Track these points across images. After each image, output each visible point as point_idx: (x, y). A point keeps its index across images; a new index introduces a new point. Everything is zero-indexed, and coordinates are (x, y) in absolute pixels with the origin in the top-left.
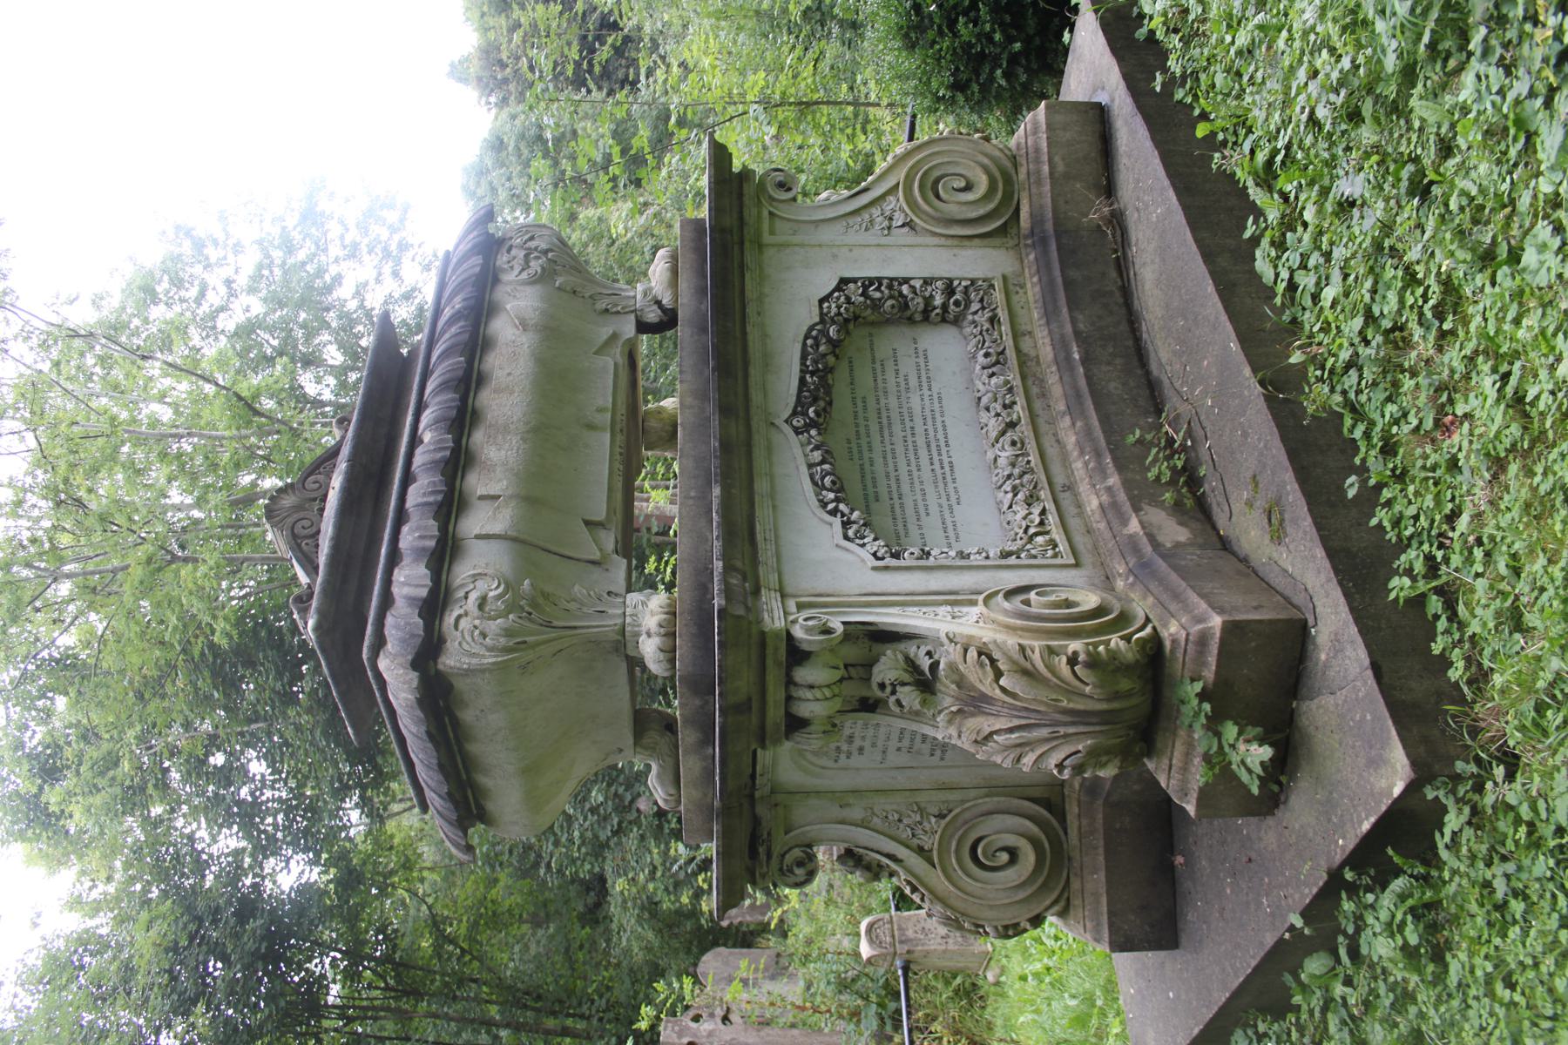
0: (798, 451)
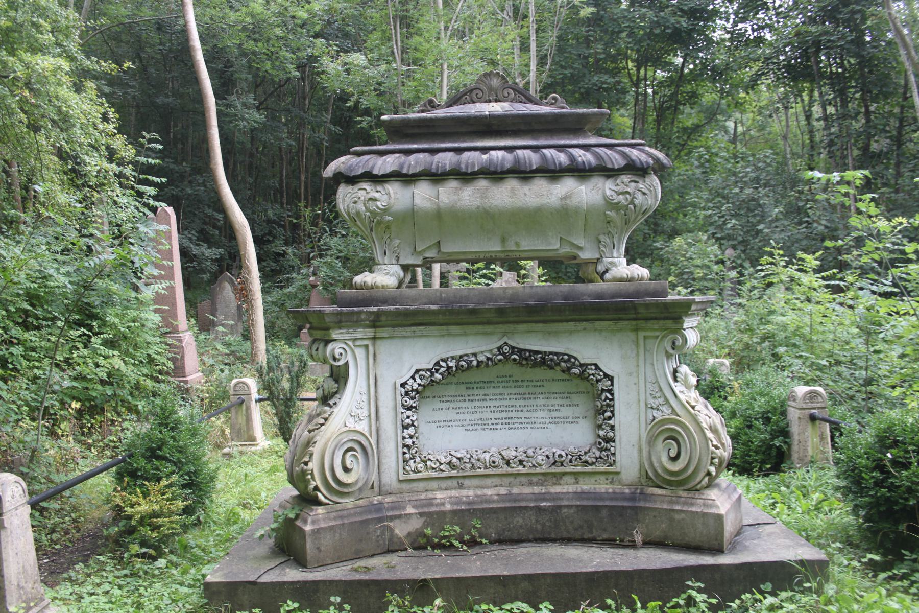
0: (483, 349)
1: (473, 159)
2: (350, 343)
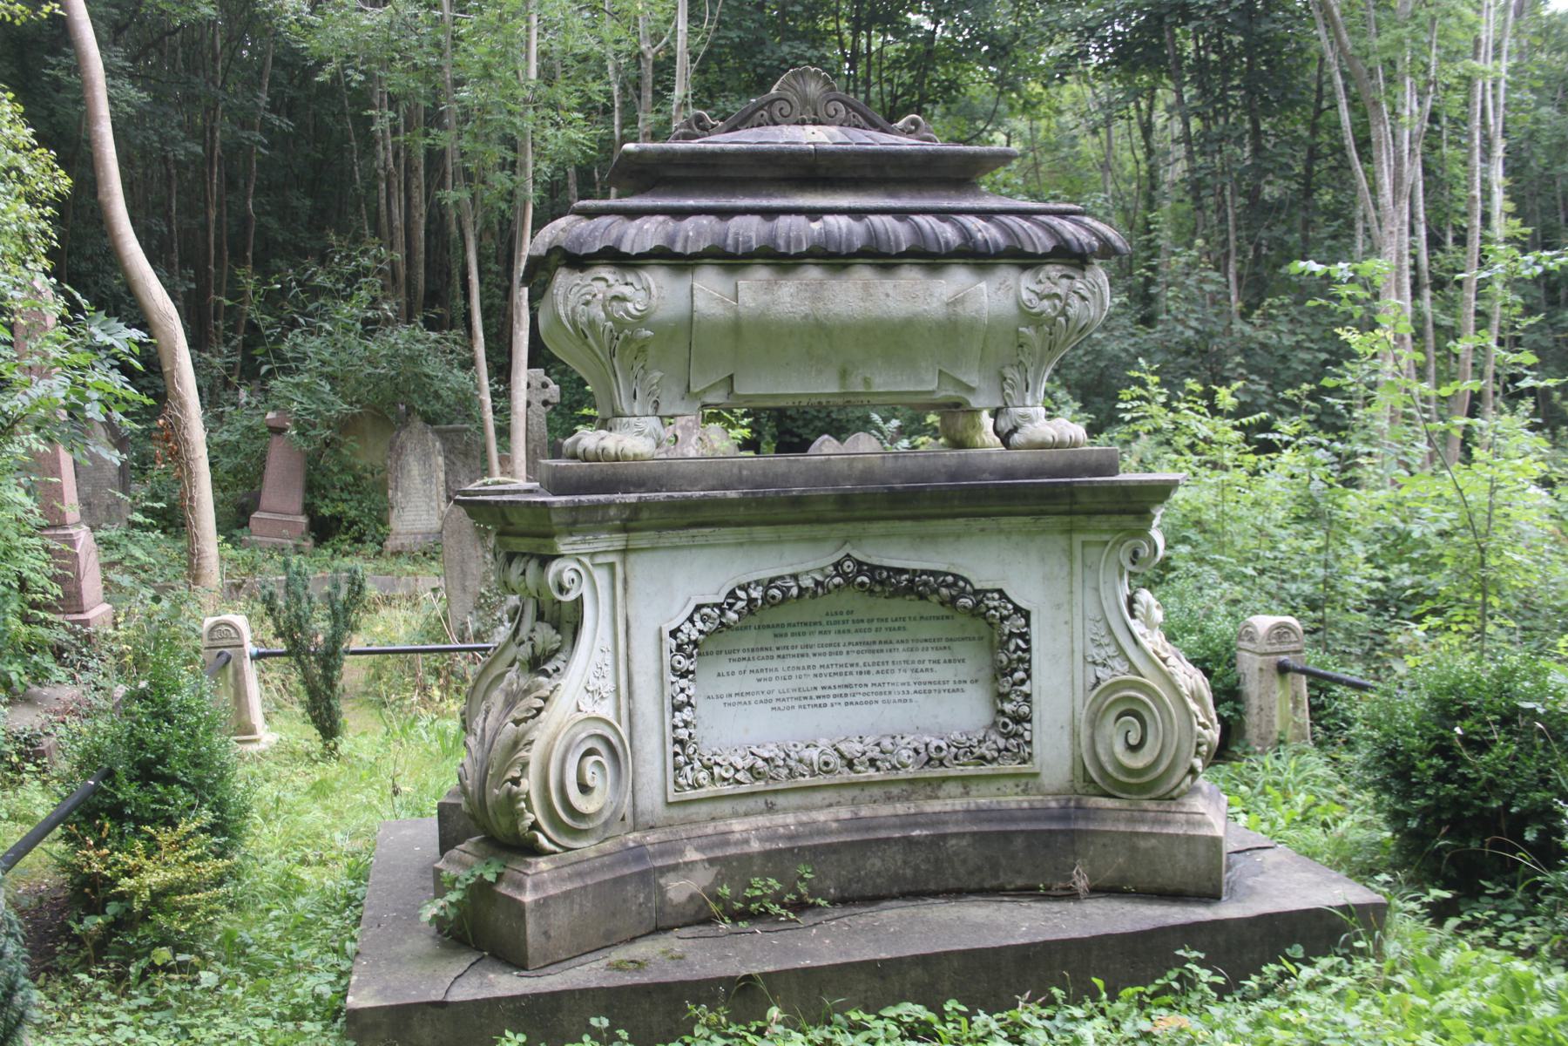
0: (810, 566)
1: (795, 230)
2: (586, 560)
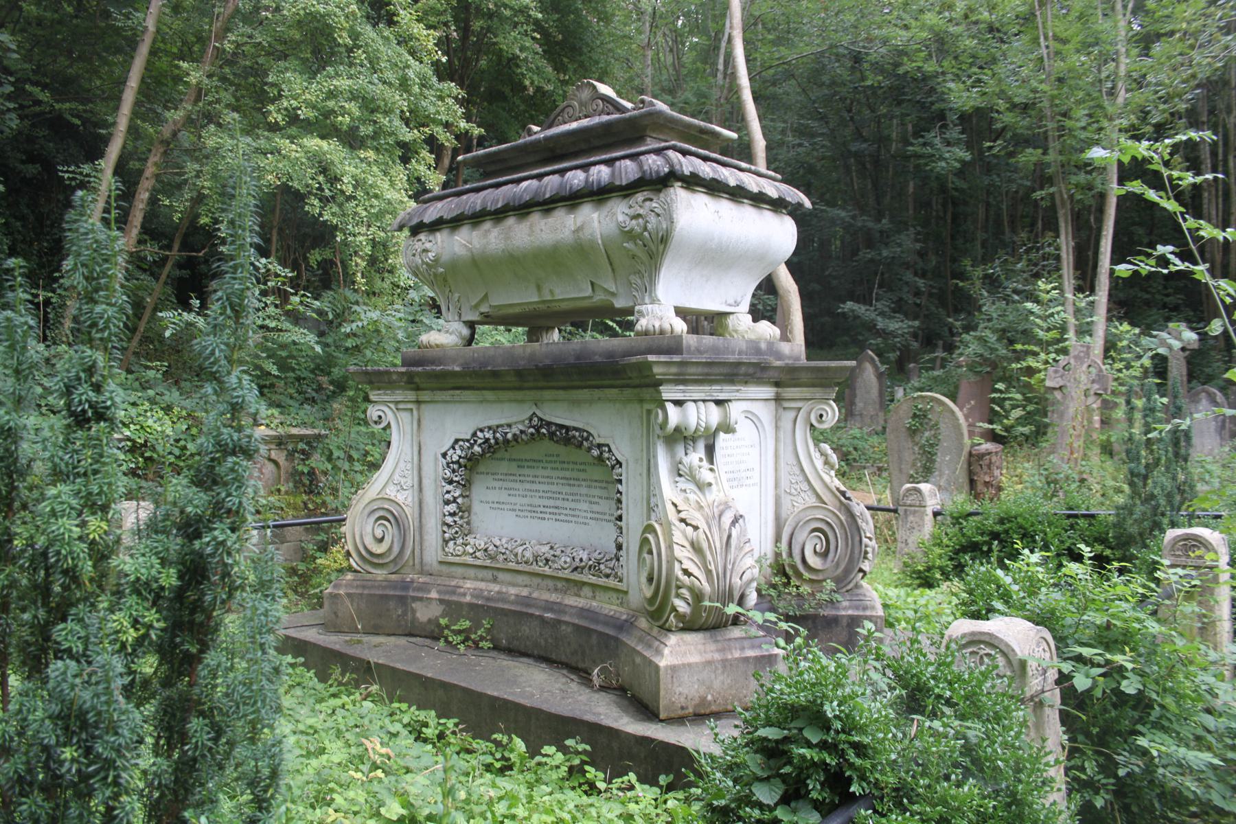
2: (392, 406)
